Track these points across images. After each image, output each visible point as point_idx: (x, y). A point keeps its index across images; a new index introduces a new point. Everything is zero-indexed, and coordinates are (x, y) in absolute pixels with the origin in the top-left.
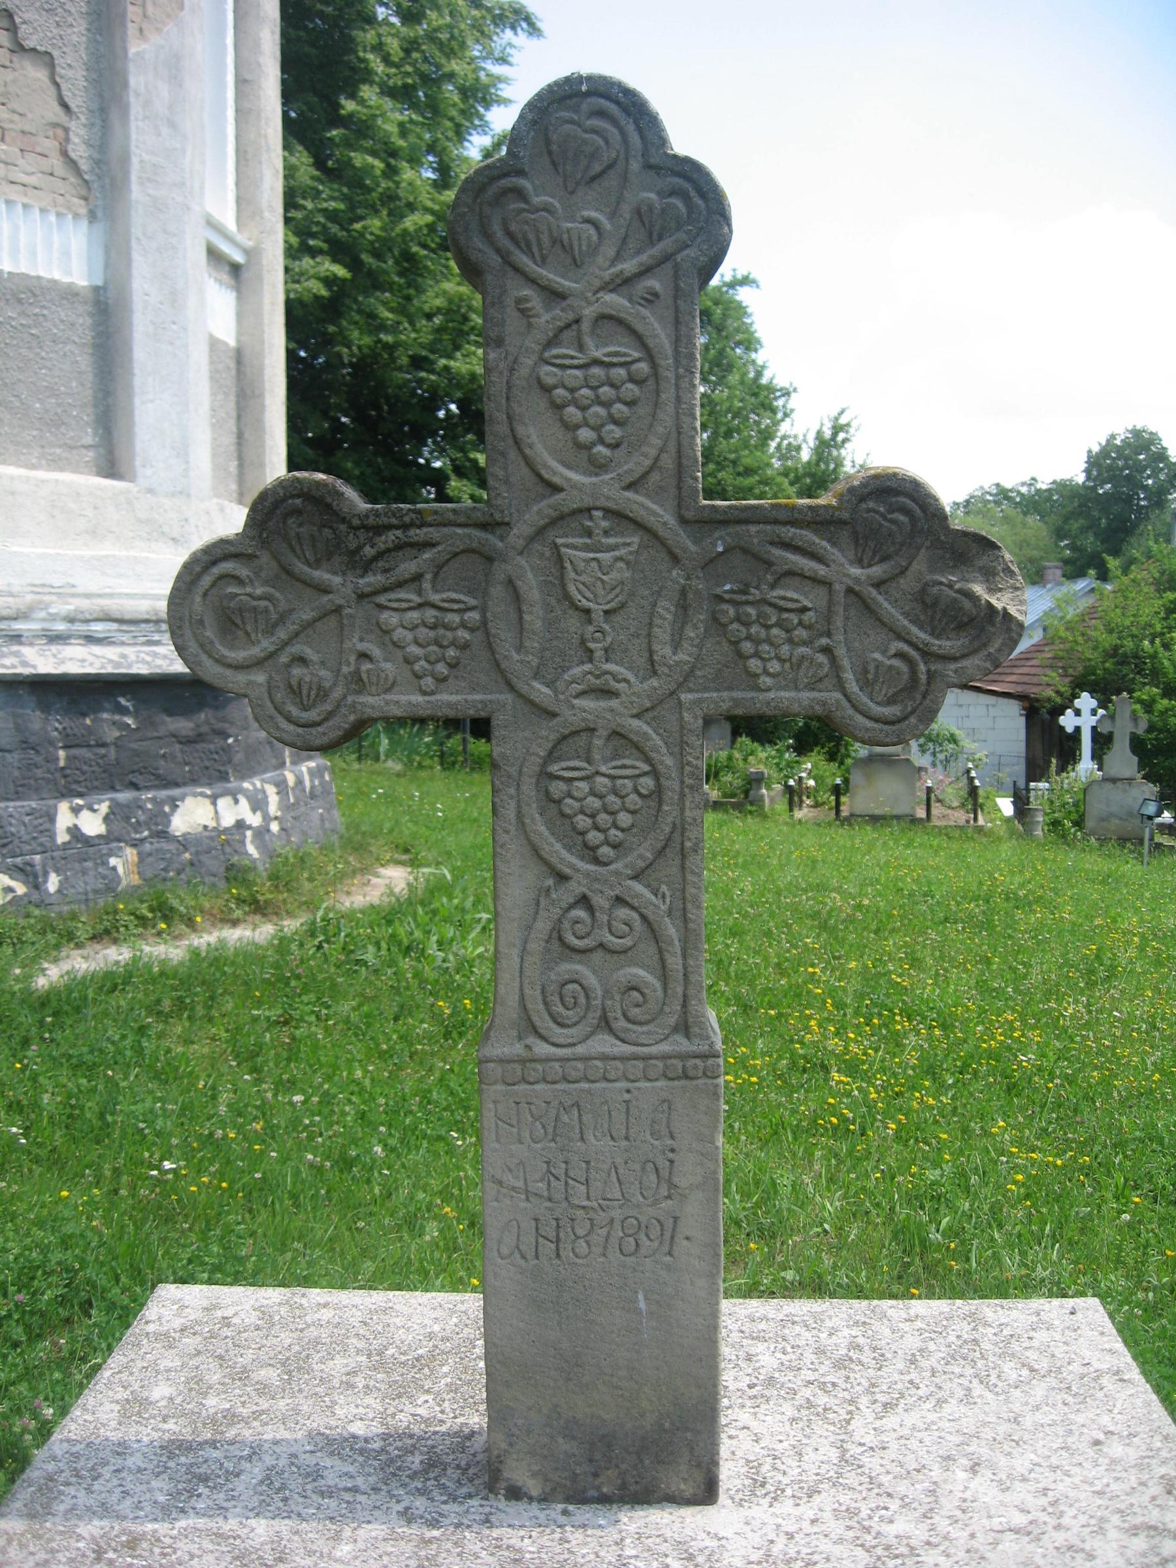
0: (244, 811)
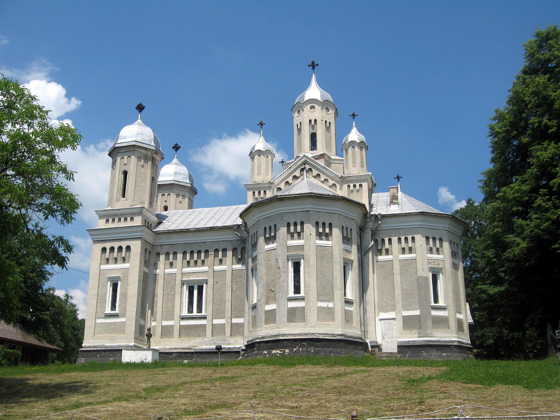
0: (279, 351)
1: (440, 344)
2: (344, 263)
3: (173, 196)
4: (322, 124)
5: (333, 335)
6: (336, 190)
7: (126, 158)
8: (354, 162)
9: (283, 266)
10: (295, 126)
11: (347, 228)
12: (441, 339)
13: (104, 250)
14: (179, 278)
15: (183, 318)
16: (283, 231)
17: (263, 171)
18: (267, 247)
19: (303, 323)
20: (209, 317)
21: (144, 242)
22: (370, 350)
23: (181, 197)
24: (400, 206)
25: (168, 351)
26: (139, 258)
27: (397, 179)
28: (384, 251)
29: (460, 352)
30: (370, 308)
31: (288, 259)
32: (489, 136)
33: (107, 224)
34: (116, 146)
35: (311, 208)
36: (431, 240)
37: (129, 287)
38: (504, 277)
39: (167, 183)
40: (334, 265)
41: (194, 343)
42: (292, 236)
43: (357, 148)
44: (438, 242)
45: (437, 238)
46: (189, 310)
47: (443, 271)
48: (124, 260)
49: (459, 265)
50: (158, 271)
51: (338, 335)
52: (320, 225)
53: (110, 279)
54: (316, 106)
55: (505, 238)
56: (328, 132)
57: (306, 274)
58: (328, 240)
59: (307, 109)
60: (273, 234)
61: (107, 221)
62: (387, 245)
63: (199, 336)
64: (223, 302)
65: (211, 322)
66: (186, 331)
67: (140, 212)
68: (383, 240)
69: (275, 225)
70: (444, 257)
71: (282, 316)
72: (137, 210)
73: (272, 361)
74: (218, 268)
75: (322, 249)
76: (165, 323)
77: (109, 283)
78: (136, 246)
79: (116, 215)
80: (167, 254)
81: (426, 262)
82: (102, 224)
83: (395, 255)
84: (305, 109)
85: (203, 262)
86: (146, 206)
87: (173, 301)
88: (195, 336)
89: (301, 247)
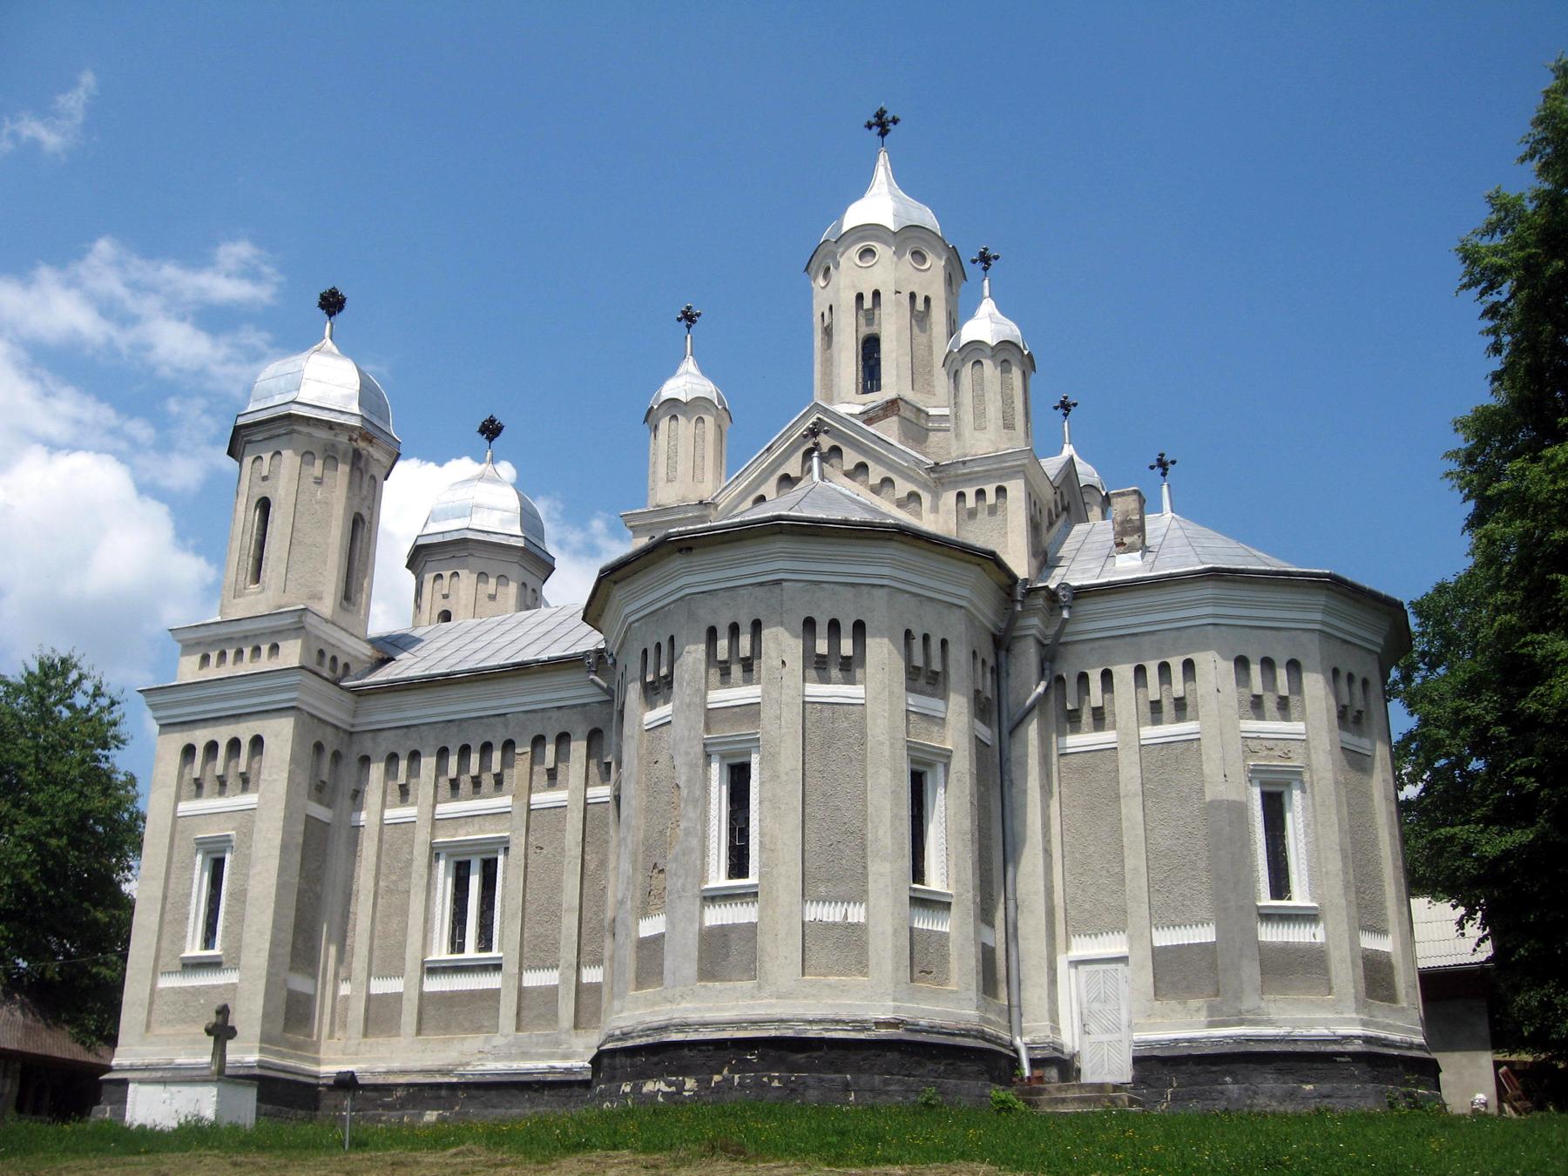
0: (662, 1086)
1: (1290, 1048)
2: (913, 761)
3: (467, 579)
4: (898, 304)
5: (861, 1025)
6: (919, 515)
7: (267, 457)
8: (979, 414)
9: (689, 780)
10: (817, 319)
11: (926, 638)
12: (1297, 1032)
13: (189, 751)
14: (422, 837)
15: (434, 970)
16: (693, 655)
17: (684, 466)
18: (652, 716)
19: (749, 984)
20: (511, 967)
21: (307, 720)
22: (1027, 1073)
23: (492, 581)
24: (1150, 557)
25: (380, 1080)
26: (285, 775)
27: (1159, 471)
28: (1086, 717)
29: (1374, 1079)
30: (1032, 925)
31: (708, 756)
32: (1464, 287)
33: (205, 670)
34: (241, 421)
35: (787, 571)
36: (1255, 670)
37: (252, 872)
38: (1538, 790)
39: (448, 538)
40: (870, 770)
41: (462, 1053)
42: (725, 671)
43: (990, 369)
44: (1282, 675)
45: (1281, 659)
46: (453, 943)
47: (1306, 777)
48: (245, 781)
49: (1372, 757)
50: (363, 815)
51: (878, 1024)
52: (822, 628)
53: (202, 844)
54: (878, 247)
55: (1525, 645)
56: (923, 329)
57: (766, 803)
58: (851, 681)
59: (850, 259)
60: (664, 671)
61: (205, 659)
62: (1096, 696)
63: (478, 1029)
64: (554, 915)
65: (514, 983)
66: (441, 1014)
67: (298, 623)
68: (1083, 678)
69: (672, 638)
70: (1308, 727)
71: (682, 959)
72: (289, 620)
73: (496, 1138)
74: (541, 798)
75: (841, 718)
76: (379, 987)
77: (199, 858)
78: (280, 735)
79: (229, 640)
80: (392, 758)
81: (1237, 746)
82: (189, 670)
83: (1124, 732)
84: (842, 261)
85: (499, 780)
86: (327, 606)
87: (404, 912)
88: (466, 1031)
89: (751, 712)
